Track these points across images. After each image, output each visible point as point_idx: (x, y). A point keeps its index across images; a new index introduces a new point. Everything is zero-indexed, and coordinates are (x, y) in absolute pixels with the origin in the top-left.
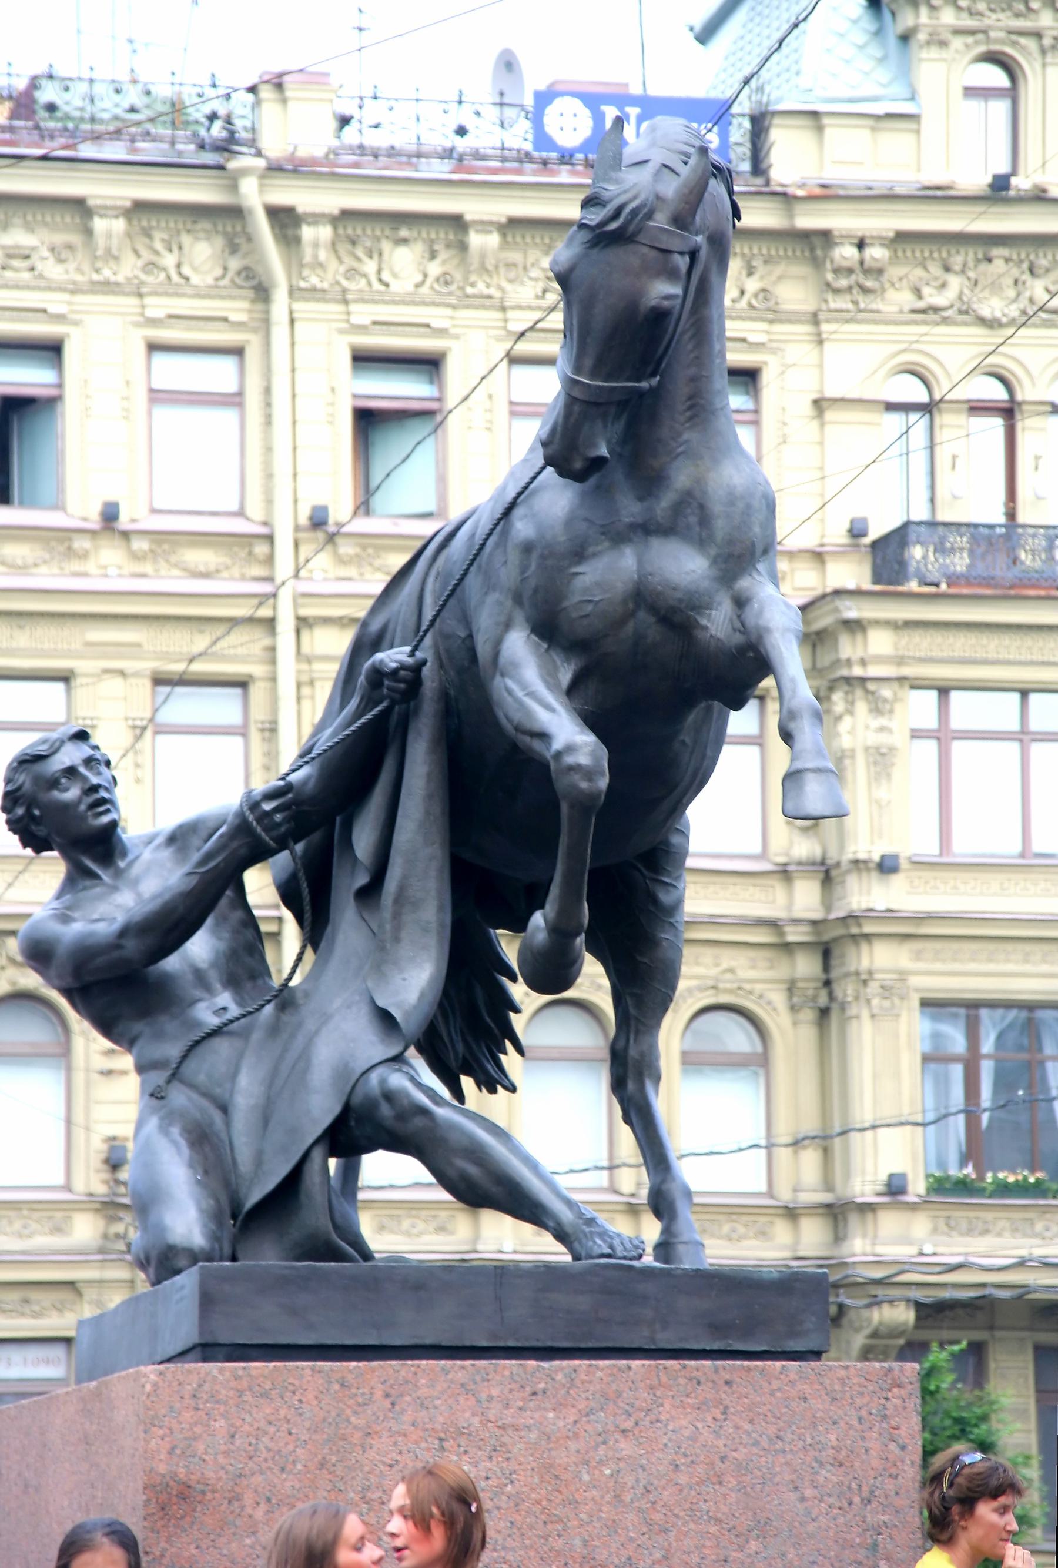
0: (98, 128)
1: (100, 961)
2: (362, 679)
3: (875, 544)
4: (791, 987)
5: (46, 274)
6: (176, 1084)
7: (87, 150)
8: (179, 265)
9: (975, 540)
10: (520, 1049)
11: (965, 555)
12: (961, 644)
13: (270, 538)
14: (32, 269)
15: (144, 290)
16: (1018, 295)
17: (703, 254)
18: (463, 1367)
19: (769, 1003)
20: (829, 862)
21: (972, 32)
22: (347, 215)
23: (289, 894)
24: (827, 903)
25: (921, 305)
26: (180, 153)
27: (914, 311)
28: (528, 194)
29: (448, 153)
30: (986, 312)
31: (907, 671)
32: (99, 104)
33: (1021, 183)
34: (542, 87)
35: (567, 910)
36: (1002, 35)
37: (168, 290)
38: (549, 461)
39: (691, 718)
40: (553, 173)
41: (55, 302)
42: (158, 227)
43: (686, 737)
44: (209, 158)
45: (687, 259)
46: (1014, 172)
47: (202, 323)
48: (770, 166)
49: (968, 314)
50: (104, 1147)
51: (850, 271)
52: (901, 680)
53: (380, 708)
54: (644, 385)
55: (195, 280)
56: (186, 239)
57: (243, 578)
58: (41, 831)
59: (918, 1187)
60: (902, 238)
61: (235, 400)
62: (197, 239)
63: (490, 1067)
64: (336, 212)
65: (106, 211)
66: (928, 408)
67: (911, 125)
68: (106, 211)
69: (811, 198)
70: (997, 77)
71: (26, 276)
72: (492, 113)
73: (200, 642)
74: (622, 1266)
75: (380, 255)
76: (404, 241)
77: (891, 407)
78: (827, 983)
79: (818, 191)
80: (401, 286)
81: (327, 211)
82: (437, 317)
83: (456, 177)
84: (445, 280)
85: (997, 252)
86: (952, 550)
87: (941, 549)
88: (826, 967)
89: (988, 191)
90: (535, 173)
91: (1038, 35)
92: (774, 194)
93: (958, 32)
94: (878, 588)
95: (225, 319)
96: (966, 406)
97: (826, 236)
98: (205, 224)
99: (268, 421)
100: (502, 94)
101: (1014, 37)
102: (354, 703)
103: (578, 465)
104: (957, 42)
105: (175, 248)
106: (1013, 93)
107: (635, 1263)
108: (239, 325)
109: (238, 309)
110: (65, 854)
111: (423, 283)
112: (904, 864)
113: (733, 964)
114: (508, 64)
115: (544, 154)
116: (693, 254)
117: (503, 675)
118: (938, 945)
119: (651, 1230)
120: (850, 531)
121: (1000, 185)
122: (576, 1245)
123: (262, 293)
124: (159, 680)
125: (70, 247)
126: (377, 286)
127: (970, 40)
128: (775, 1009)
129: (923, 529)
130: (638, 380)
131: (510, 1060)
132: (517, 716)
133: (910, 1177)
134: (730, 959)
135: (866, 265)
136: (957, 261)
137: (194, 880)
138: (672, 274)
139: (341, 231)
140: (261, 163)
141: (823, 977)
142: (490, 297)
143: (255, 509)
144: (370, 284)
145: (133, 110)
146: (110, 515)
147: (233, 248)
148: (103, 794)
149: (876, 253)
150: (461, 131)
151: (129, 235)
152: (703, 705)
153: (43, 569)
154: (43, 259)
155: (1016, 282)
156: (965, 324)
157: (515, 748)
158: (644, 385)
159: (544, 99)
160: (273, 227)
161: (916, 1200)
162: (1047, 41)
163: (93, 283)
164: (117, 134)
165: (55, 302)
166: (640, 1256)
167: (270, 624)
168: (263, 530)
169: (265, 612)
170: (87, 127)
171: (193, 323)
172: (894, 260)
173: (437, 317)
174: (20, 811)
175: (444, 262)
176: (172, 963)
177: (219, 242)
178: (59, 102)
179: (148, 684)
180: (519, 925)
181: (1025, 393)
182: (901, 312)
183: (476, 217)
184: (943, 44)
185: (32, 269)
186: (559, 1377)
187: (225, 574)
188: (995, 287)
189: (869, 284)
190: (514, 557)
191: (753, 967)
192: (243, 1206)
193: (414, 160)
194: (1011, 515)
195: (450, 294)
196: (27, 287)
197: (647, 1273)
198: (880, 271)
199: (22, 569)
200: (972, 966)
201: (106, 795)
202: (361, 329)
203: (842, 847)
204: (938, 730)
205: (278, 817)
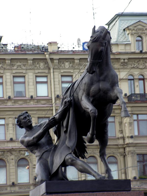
0: (29, 50)
1: (30, 142)
2: (64, 103)
3: (128, 97)
4: (120, 153)
5: (23, 68)
6: (29, 79)
7: (27, 52)
8: (39, 66)
9: (140, 96)
10: (87, 153)
11: (139, 98)
12: (139, 109)
13: (52, 99)
14: (21, 67)
15: (35, 69)
16: (144, 65)
17: (107, 43)
18: (82, 194)
19: (118, 155)
20: (124, 137)
21: (137, 33)
22: (60, 59)
23: (55, 133)
24: (124, 142)
25: (132, 67)
26: (39, 52)
27: (131, 68)
28: (82, 55)
29: (72, 51)
30: (140, 67)
31: (133, 112)
32: (29, 47)
33: (144, 51)
34: (84, 42)
35: (92, 135)
36: (140, 33)
37: (38, 69)
38: (88, 72)
39: (108, 105)
40: (85, 52)
41: (24, 72)
42: (36, 62)
43: (107, 108)
44: (42, 53)
45: (105, 44)
46: (143, 50)
47: (42, 73)
48: (112, 51)
49: (138, 68)
50: (34, 177)
51: (123, 63)
52: (132, 114)
53: (66, 106)
54: (100, 61)
55: (41, 68)
56: (40, 63)
57: (49, 104)
58: (22, 125)
59: (138, 178)
60: (129, 59)
61: (46, 82)
62: (41, 63)
63: (83, 155)
64: (58, 58)
65: (30, 60)
66: (133, 79)
67: (129, 45)
68: (30, 60)
69: (117, 54)
70: (140, 39)
71: (20, 68)
72: (77, 46)
73: (44, 113)
74: (103, 180)
75: (64, 64)
76: (67, 62)
77: (129, 80)
78: (125, 152)
79: (118, 53)
80: (67, 67)
81: (57, 58)
82: (72, 71)
83: (73, 53)
84: (72, 66)
85: (141, 60)
86: (138, 97)
87: (136, 97)
88: (124, 150)
89: (140, 52)
90: (83, 53)
91: (144, 33)
92: (113, 54)
93: (135, 33)
94: (129, 102)
95: (45, 72)
96: (138, 79)
97: (119, 59)
98: (42, 61)
99: (51, 85)
100: (78, 43)
101: (142, 34)
102: (63, 106)
103: (91, 72)
104: (135, 34)
105: (39, 64)
106: (142, 41)
107: (104, 179)
108: (47, 73)
109: (47, 71)
110: (25, 129)
111: (69, 67)
112: (134, 137)
113: (112, 150)
114: (79, 40)
115: (84, 50)
116: (106, 43)
117: (83, 101)
118: (139, 147)
119: (107, 175)
120: (125, 95)
121: (141, 52)
122: (96, 177)
123: (49, 69)
124: (39, 118)
125: (25, 64)
126: (64, 67)
127: (136, 34)
128: (118, 156)
129: (134, 95)
130: (99, 60)
131: (86, 155)
132: (85, 106)
133: (137, 177)
134: (112, 150)
135: (125, 62)
136: (136, 61)
137: (43, 130)
138: (103, 46)
139: (59, 61)
140: (49, 53)
141: (124, 152)
142: (78, 68)
143: (50, 96)
144: (63, 67)
145: (33, 47)
146: (32, 97)
147: (45, 64)
148: (30, 120)
149: (126, 61)
150: (74, 48)
151: (33, 63)
152: (109, 104)
153: (24, 105)
154: (22, 66)
155: (144, 64)
156: (138, 69)
157: (85, 111)
158: (100, 61)
159: (84, 44)
160: (51, 61)
161: (137, 180)
162: (146, 34)
163: (29, 69)
164: (31, 50)
165: (24, 72)
166: (105, 178)
167: (52, 110)
168: (51, 98)
169: (51, 109)
170: (27, 50)
171: (41, 73)
172: (128, 61)
173: (72, 71)
174: (19, 123)
175: (72, 64)
176: (40, 142)
177: (44, 63)
178: (24, 47)
179: (37, 118)
180: (86, 135)
181: (145, 77)
182: (130, 68)
183: (76, 58)
184: (133, 35)
185: (21, 67)
186: (95, 195)
187: (46, 104)
188: (141, 64)
189: (125, 64)
190: (83, 85)
191: (115, 151)
192: (51, 173)
193: (68, 52)
194: (145, 92)
195: (73, 68)
196: (20, 70)
197: (106, 180)
198: (127, 63)
199: (21, 105)
200: (143, 150)
201: (30, 120)
202: (62, 73)
203: (126, 135)
204: (137, 120)
205: (53, 122)
